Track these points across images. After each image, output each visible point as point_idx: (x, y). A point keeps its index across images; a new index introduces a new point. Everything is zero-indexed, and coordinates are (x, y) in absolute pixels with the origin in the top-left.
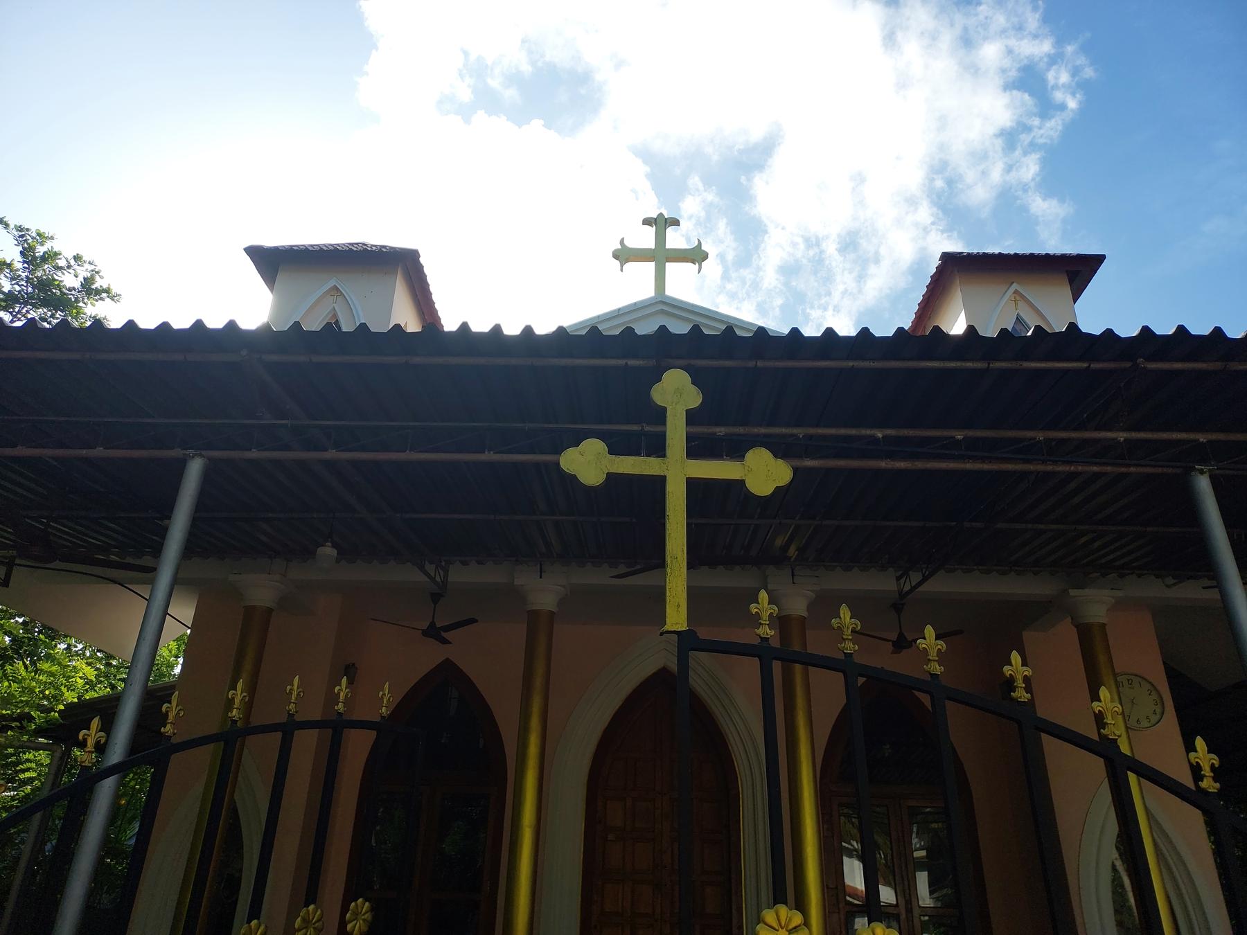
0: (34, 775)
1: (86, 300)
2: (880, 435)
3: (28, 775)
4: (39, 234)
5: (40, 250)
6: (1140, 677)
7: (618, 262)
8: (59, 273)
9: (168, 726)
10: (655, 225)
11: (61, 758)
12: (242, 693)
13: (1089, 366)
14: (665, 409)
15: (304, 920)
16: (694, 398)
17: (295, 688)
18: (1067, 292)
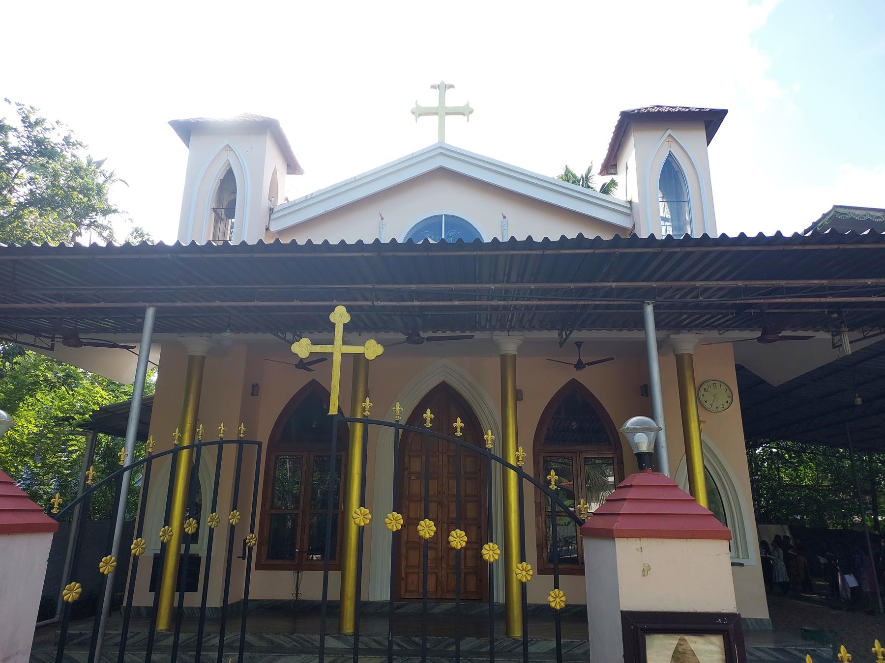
0: (76, 448)
1: (67, 150)
2: (493, 287)
3: (73, 448)
4: (32, 108)
5: (33, 119)
6: (721, 382)
7: (413, 116)
8: (47, 133)
9: (150, 449)
10: (439, 89)
11: (92, 439)
12: (178, 433)
13: (594, 252)
14: (335, 324)
15: (211, 518)
16: (347, 318)
17: (201, 429)
18: (703, 135)
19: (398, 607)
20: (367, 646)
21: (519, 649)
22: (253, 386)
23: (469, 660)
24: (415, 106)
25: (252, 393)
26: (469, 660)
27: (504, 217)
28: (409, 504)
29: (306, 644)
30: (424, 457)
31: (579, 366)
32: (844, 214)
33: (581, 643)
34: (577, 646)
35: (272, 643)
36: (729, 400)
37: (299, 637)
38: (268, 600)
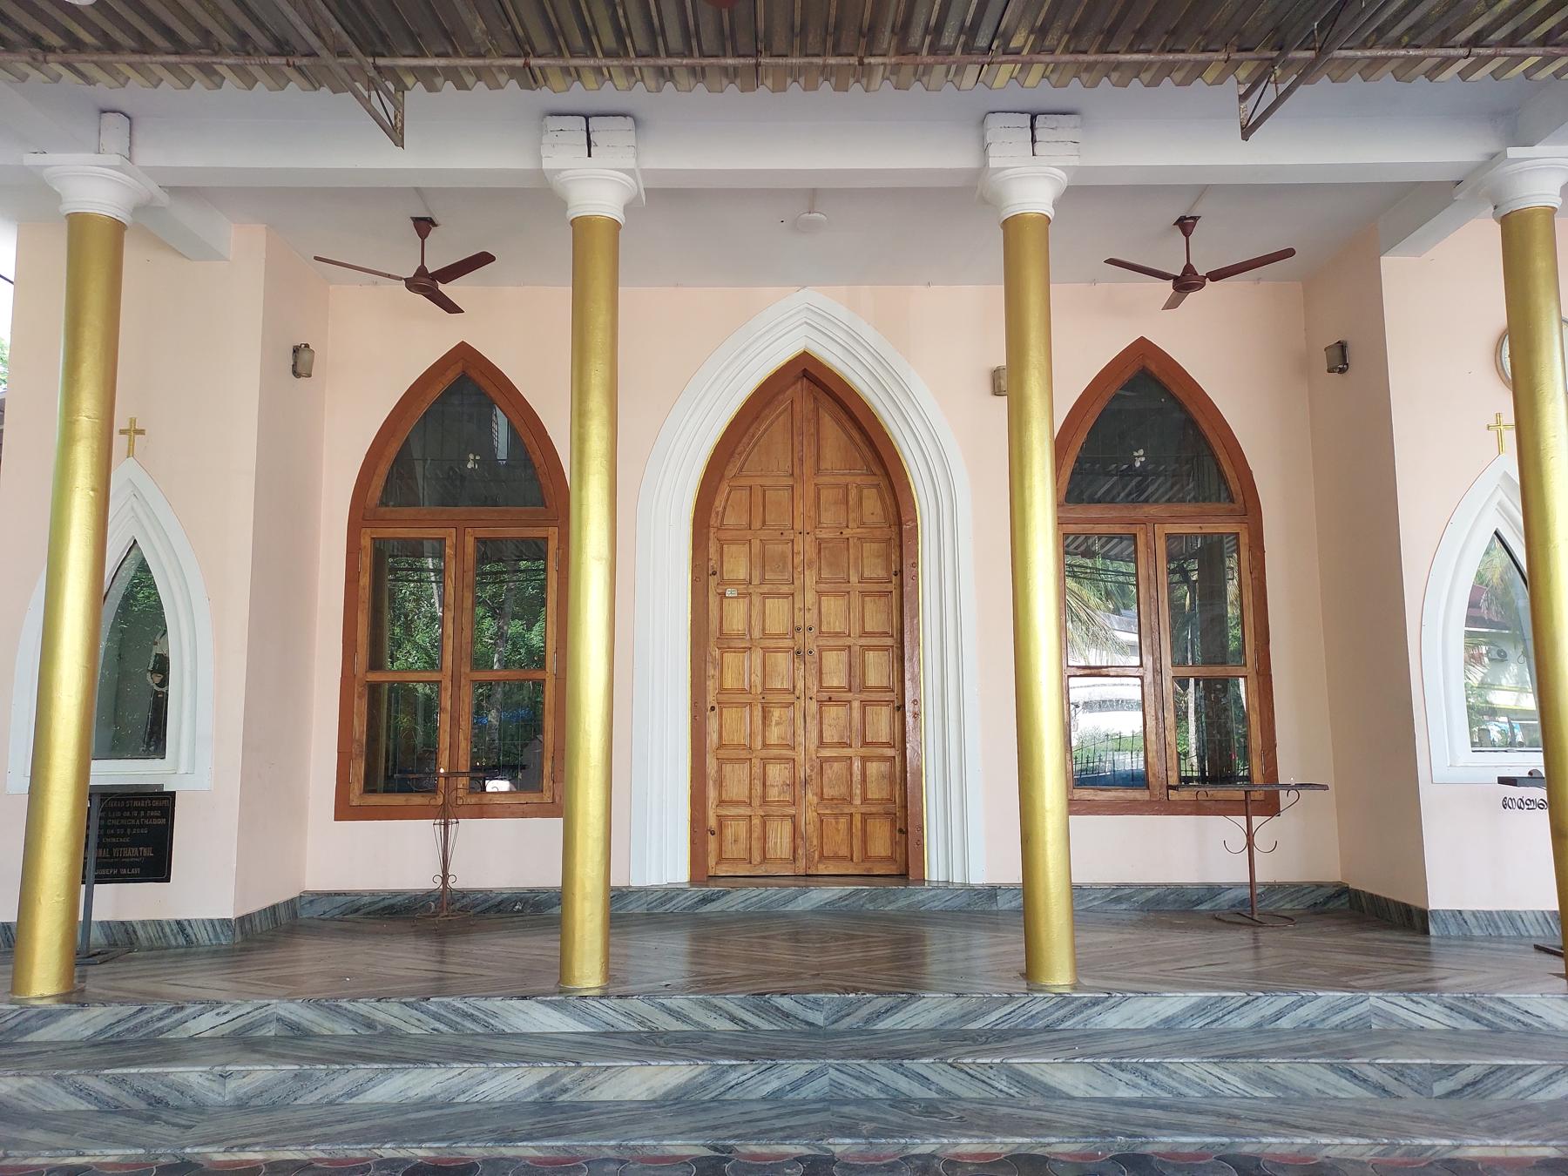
19: (706, 900)
20: (644, 1026)
21: (1075, 1020)
22: (296, 350)
23: (950, 1065)
25: (294, 366)
26: (950, 1065)
28: (722, 658)
29: (468, 1024)
30: (756, 544)
33: (1246, 1000)
34: (1238, 1008)
35: (370, 1024)
37: (446, 1006)
38: (373, 893)
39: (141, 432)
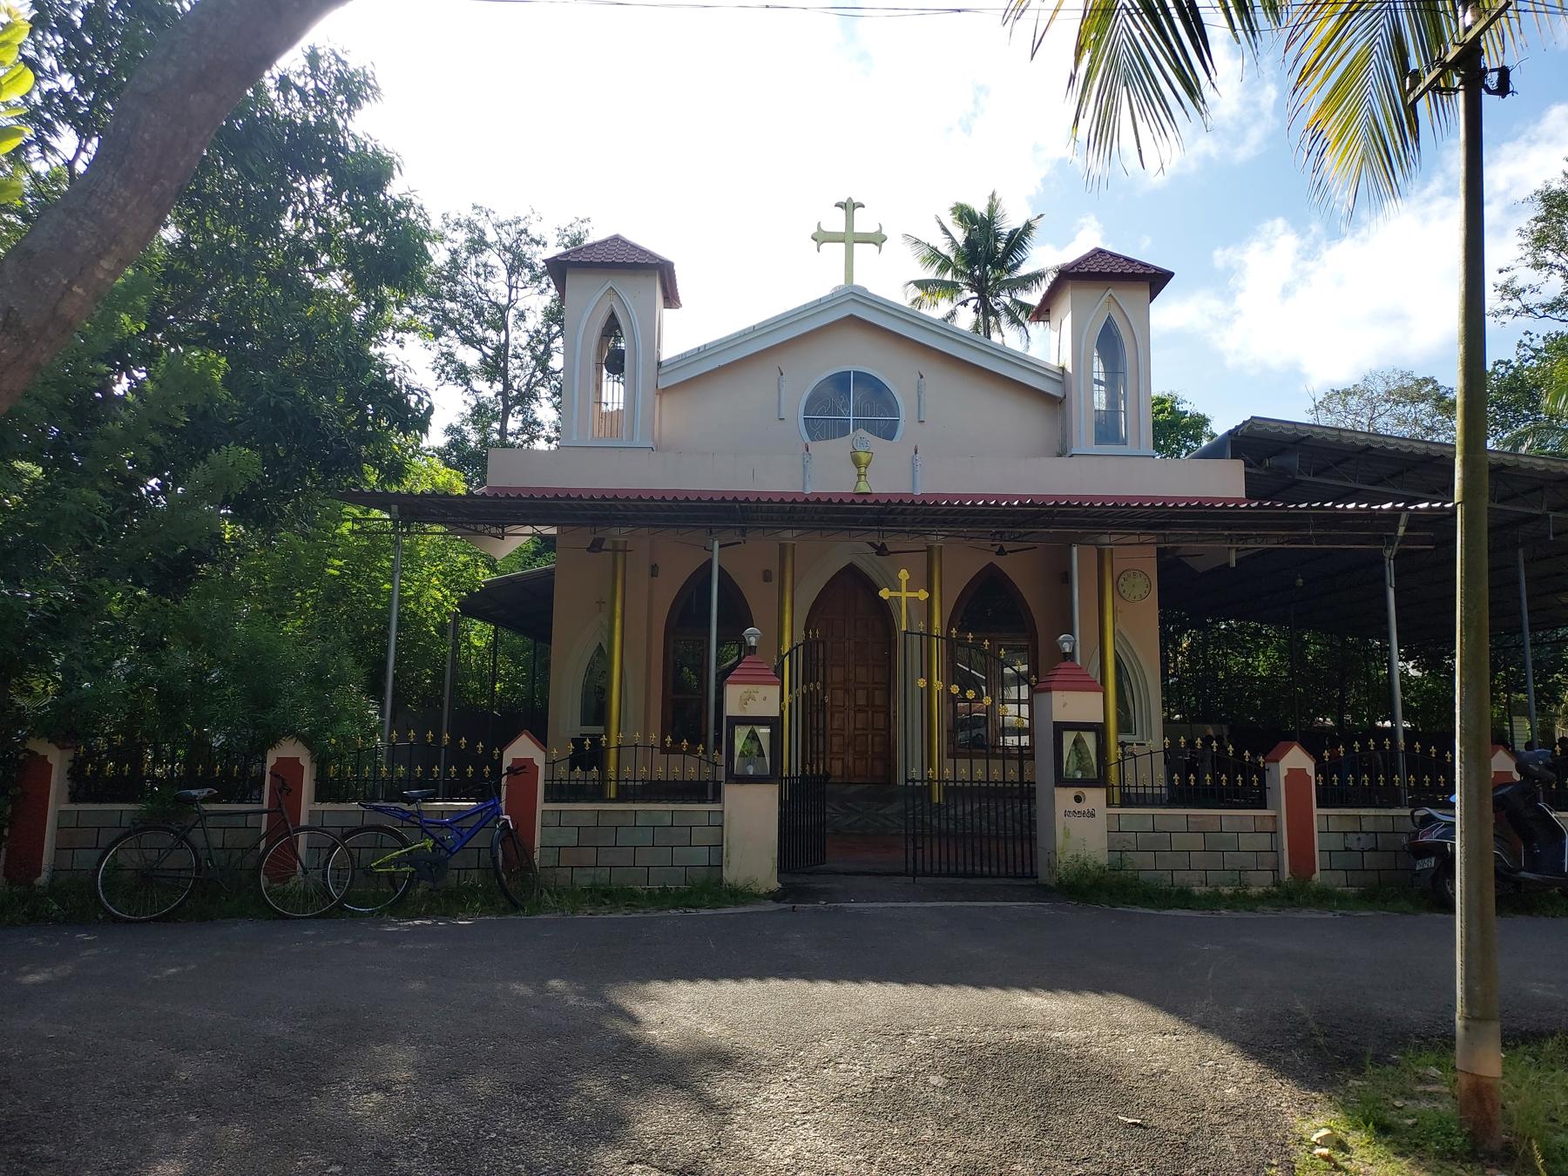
24: (816, 230)
27: (922, 377)
31: (1001, 552)
32: (1260, 425)
36: (1147, 590)
39: (597, 602)
